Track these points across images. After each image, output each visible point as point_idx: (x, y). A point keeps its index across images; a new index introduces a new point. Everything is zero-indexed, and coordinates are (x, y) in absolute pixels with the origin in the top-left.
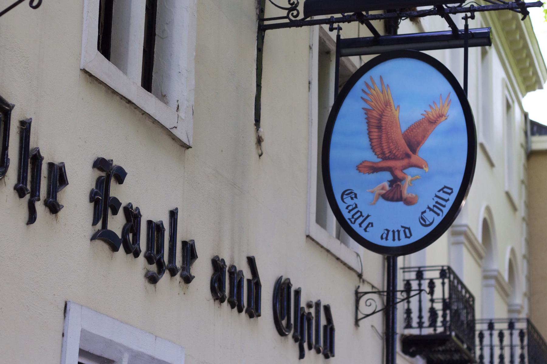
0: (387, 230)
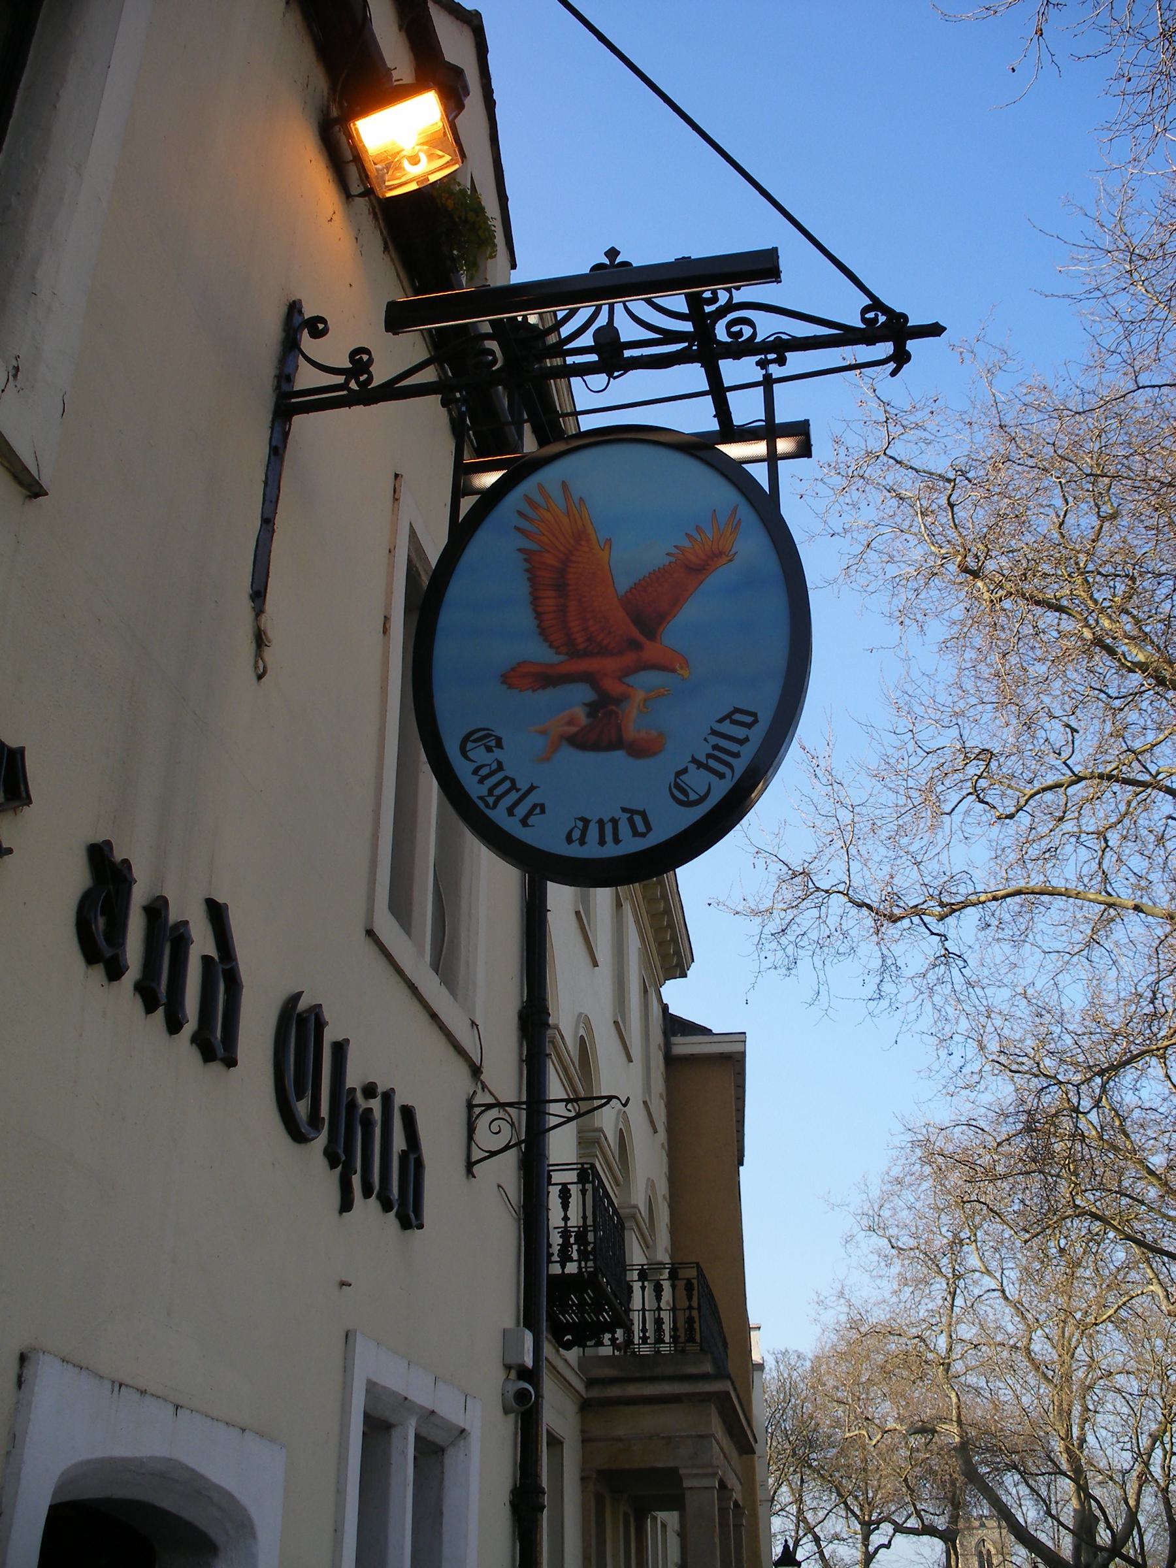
0: (582, 819)
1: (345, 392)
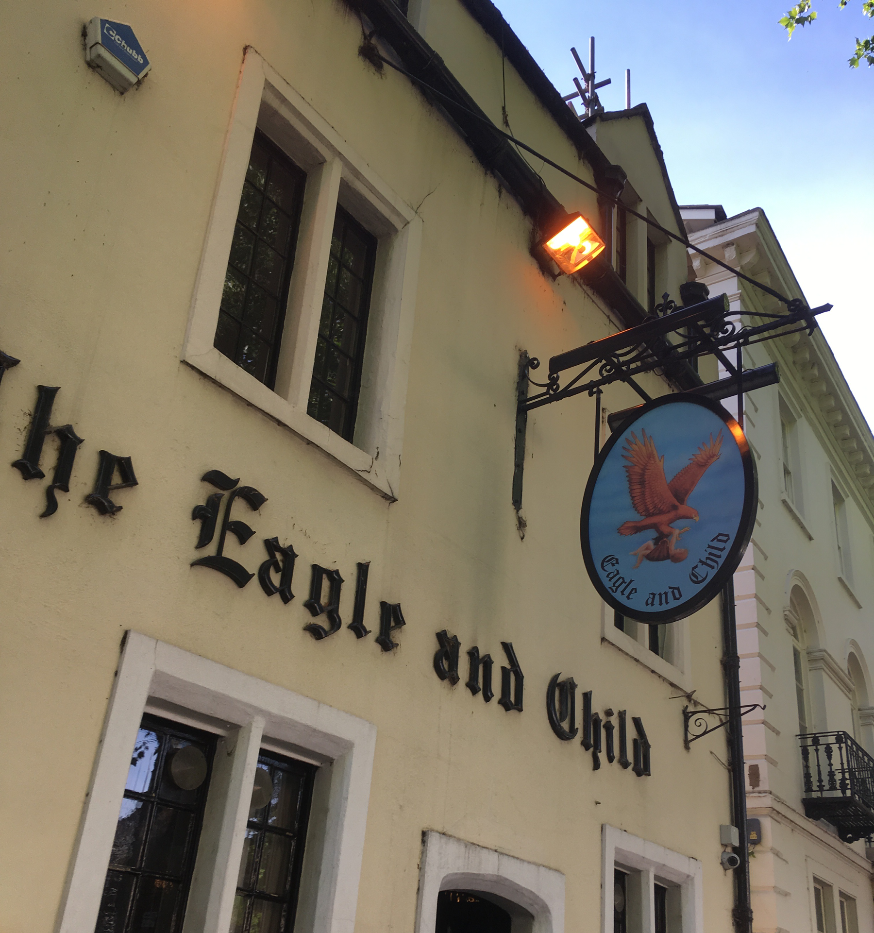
0: (652, 594)
1: (548, 396)
